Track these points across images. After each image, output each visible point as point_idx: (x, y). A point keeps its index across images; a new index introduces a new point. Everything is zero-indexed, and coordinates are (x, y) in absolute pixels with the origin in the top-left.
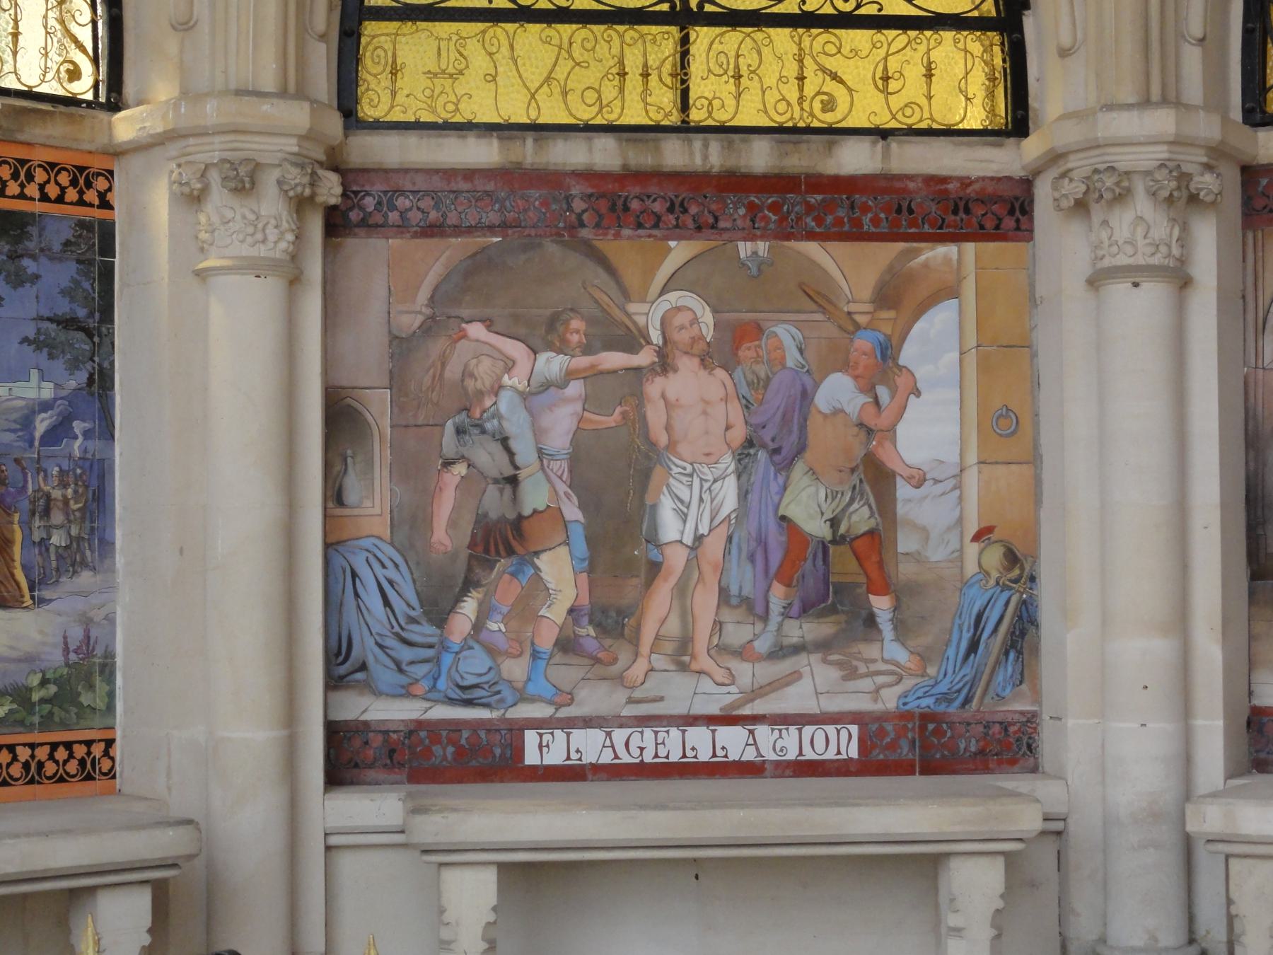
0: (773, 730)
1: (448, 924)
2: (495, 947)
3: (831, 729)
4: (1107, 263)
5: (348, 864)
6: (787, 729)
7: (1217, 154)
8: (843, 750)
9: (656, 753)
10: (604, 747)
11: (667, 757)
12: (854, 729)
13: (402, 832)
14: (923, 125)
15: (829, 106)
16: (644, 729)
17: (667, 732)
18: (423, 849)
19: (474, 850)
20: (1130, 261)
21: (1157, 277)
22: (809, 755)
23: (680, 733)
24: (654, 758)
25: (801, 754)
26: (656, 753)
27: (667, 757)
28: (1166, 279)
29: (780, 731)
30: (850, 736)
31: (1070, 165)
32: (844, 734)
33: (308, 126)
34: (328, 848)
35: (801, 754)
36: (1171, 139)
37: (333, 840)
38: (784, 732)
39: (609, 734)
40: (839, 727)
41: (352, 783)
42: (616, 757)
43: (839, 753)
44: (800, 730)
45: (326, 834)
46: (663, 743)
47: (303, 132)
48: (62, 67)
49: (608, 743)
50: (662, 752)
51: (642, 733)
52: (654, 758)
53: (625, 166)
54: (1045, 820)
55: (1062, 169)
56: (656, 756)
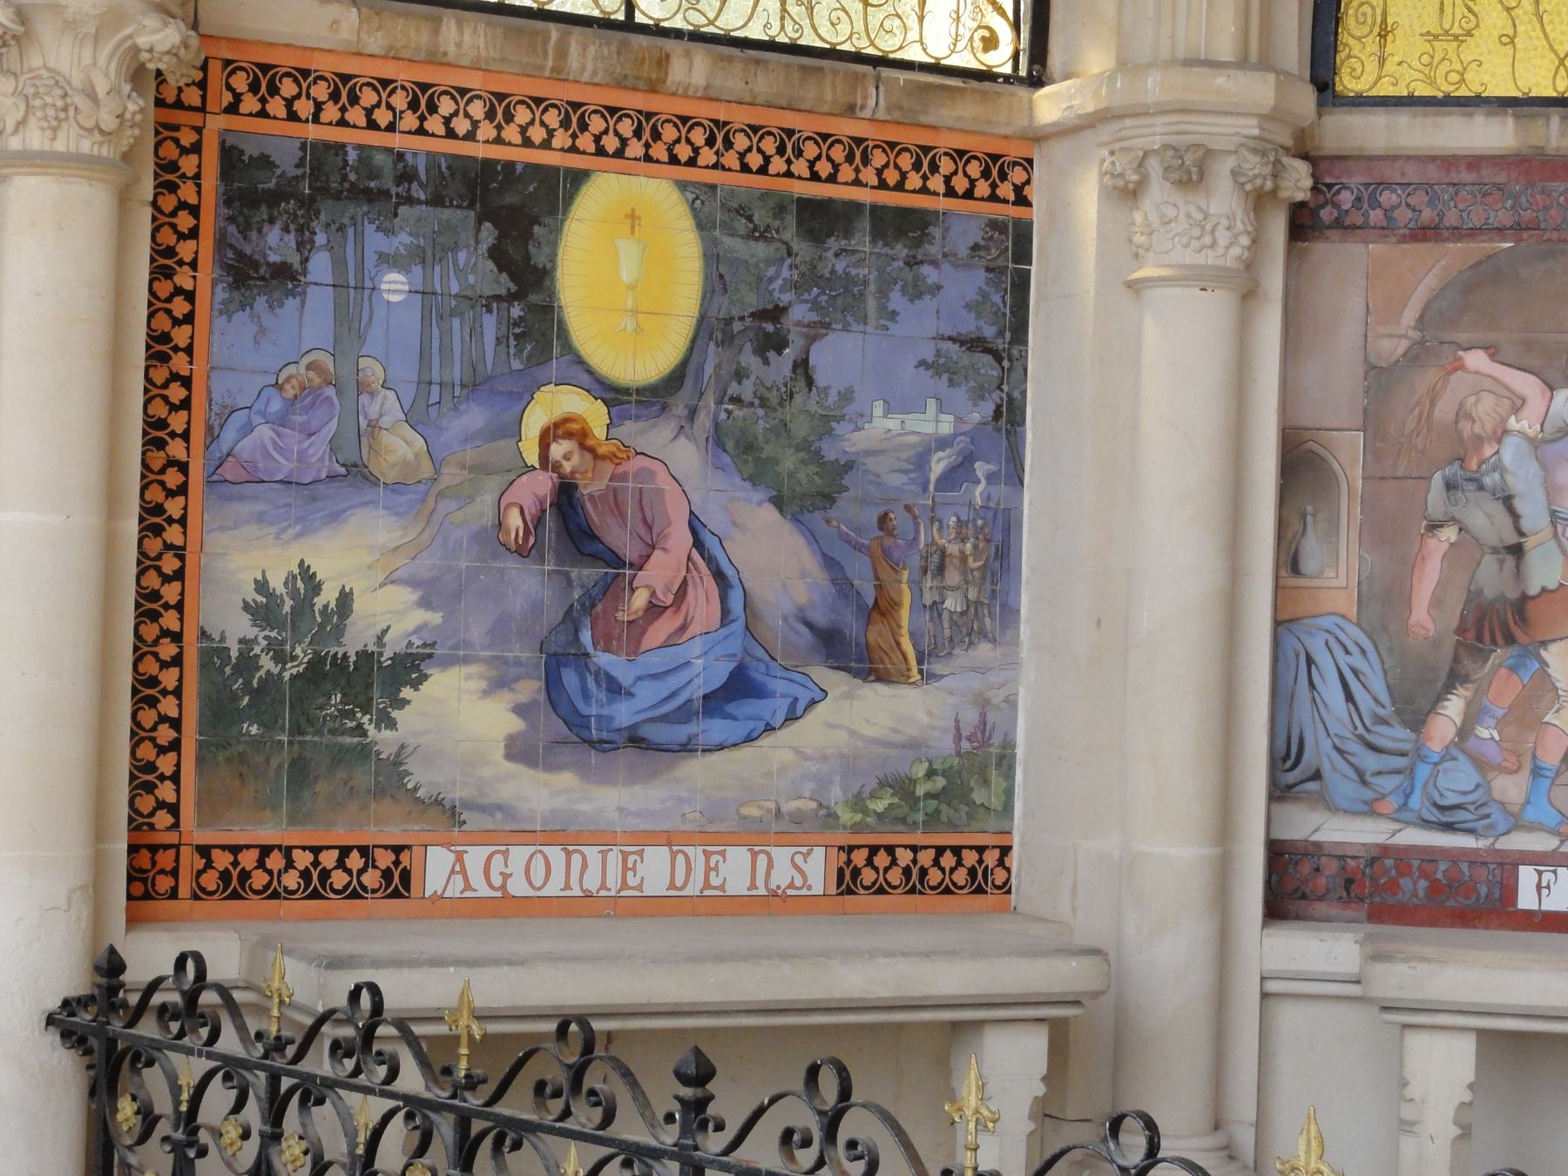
8: (760, 882)
10: (453, 872)
34: (1265, 996)
37: (1272, 986)
39: (460, 858)
45: (1263, 979)
49: (458, 868)
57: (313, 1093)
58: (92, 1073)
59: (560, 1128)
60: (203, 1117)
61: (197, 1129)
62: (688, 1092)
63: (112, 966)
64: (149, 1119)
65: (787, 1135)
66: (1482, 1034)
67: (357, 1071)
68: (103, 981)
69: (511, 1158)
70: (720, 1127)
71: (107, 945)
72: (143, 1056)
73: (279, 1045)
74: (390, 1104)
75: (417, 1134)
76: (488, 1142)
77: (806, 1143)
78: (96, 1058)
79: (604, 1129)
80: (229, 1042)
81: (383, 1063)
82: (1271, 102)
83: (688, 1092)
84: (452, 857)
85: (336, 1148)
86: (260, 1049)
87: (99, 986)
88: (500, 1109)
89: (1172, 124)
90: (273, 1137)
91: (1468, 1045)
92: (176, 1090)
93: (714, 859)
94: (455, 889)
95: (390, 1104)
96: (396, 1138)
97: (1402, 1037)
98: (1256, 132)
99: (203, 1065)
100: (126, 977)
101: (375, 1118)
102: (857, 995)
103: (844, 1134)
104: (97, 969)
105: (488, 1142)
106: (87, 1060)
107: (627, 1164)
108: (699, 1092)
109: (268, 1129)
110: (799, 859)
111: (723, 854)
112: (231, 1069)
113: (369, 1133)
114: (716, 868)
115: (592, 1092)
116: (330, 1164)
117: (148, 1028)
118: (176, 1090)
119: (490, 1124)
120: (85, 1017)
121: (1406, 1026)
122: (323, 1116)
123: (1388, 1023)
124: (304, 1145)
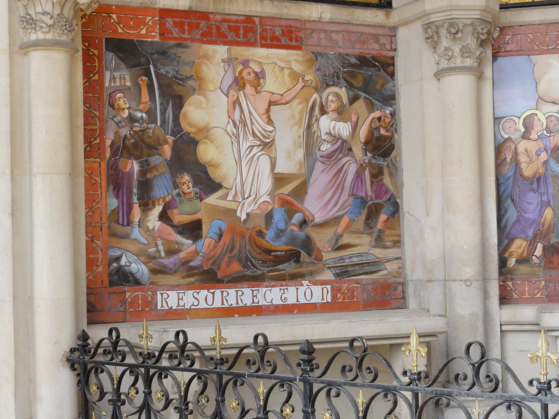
0: (280, 289)
5: (511, 338)
6: (287, 289)
8: (325, 298)
9: (179, 303)
12: (329, 287)
13: (538, 324)
17: (258, 290)
19: (398, 338)
22: (302, 301)
23: (220, 292)
26: (179, 303)
27: (258, 303)
29: (284, 289)
30: (328, 292)
32: (325, 290)
33: (485, 4)
37: (505, 328)
38: (286, 290)
40: (323, 286)
41: (507, 304)
43: (323, 299)
45: (501, 325)
46: (182, 299)
47: (482, 8)
51: (270, 290)
53: (190, 7)
54: (420, 336)
57: (163, 373)
58: (78, 378)
59: (353, 383)
60: (122, 390)
61: (121, 394)
62: (305, 357)
63: (84, 337)
64: (102, 394)
65: (344, 368)
67: (180, 364)
68: (80, 343)
69: (240, 388)
70: (318, 367)
71: (81, 330)
72: (99, 368)
73: (223, 361)
74: (124, 368)
75: (202, 384)
76: (156, 377)
77: (351, 370)
78: (78, 371)
79: (155, 364)
80: (130, 360)
81: (189, 359)
83: (305, 357)
85: (251, 404)
86: (141, 359)
87: (78, 345)
88: (233, 370)
90: (220, 401)
92: (257, 397)
93: (255, 293)
95: (124, 368)
96: (195, 386)
99: (121, 369)
100: (89, 341)
101: (119, 374)
103: (365, 365)
104: (79, 338)
105: (156, 377)
106: (76, 372)
107: (282, 386)
108: (310, 357)
109: (147, 391)
110: (195, 294)
112: (132, 368)
113: (185, 386)
114: (256, 296)
115: (268, 362)
116: (106, 393)
117: (100, 358)
118: (112, 379)
119: (231, 377)
120: (77, 354)
122: (168, 382)
124: (162, 393)
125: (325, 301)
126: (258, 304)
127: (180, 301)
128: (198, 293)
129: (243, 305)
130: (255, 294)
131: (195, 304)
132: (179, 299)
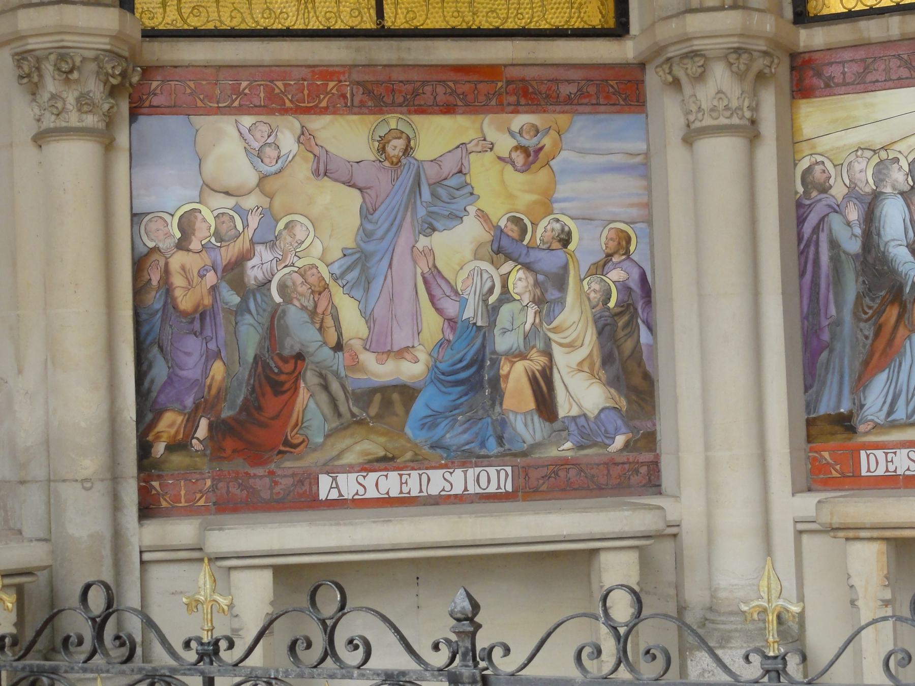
1: (237, 616)
2: (273, 632)
3: (880, 453)
4: (697, 124)
5: (157, 574)
7: (775, 43)
8: (502, 486)
10: (331, 488)
11: (409, 493)
14: (210, 26)
15: (168, 16)
16: (389, 473)
17: (895, 453)
18: (3, 574)
20: (715, 123)
21: (728, 132)
24: (419, 493)
25: (466, 489)
27: (409, 493)
28: (98, 139)
30: (507, 474)
31: (669, 55)
32: (503, 474)
34: (142, 562)
35: (466, 489)
36: (739, 31)
37: (147, 556)
39: (335, 479)
40: (499, 468)
42: (341, 495)
43: (421, 491)
44: (465, 473)
45: (141, 552)
46: (892, 461)
48: (160, 19)
49: (334, 485)
50: (891, 468)
52: (419, 493)
55: (664, 58)
56: (887, 471)
66: (277, 570)
82: (117, 28)
84: (331, 479)
89: (678, 50)
91: (268, 575)
94: (334, 495)
97: (229, 574)
98: (108, 47)
102: (14, 567)
111: (409, 475)
121: (230, 568)
123: (220, 567)
125: (425, 494)
126: (410, 494)
127: (404, 486)
128: (364, 477)
129: (377, 495)
130: (404, 481)
131: (911, 469)
132: (402, 484)
